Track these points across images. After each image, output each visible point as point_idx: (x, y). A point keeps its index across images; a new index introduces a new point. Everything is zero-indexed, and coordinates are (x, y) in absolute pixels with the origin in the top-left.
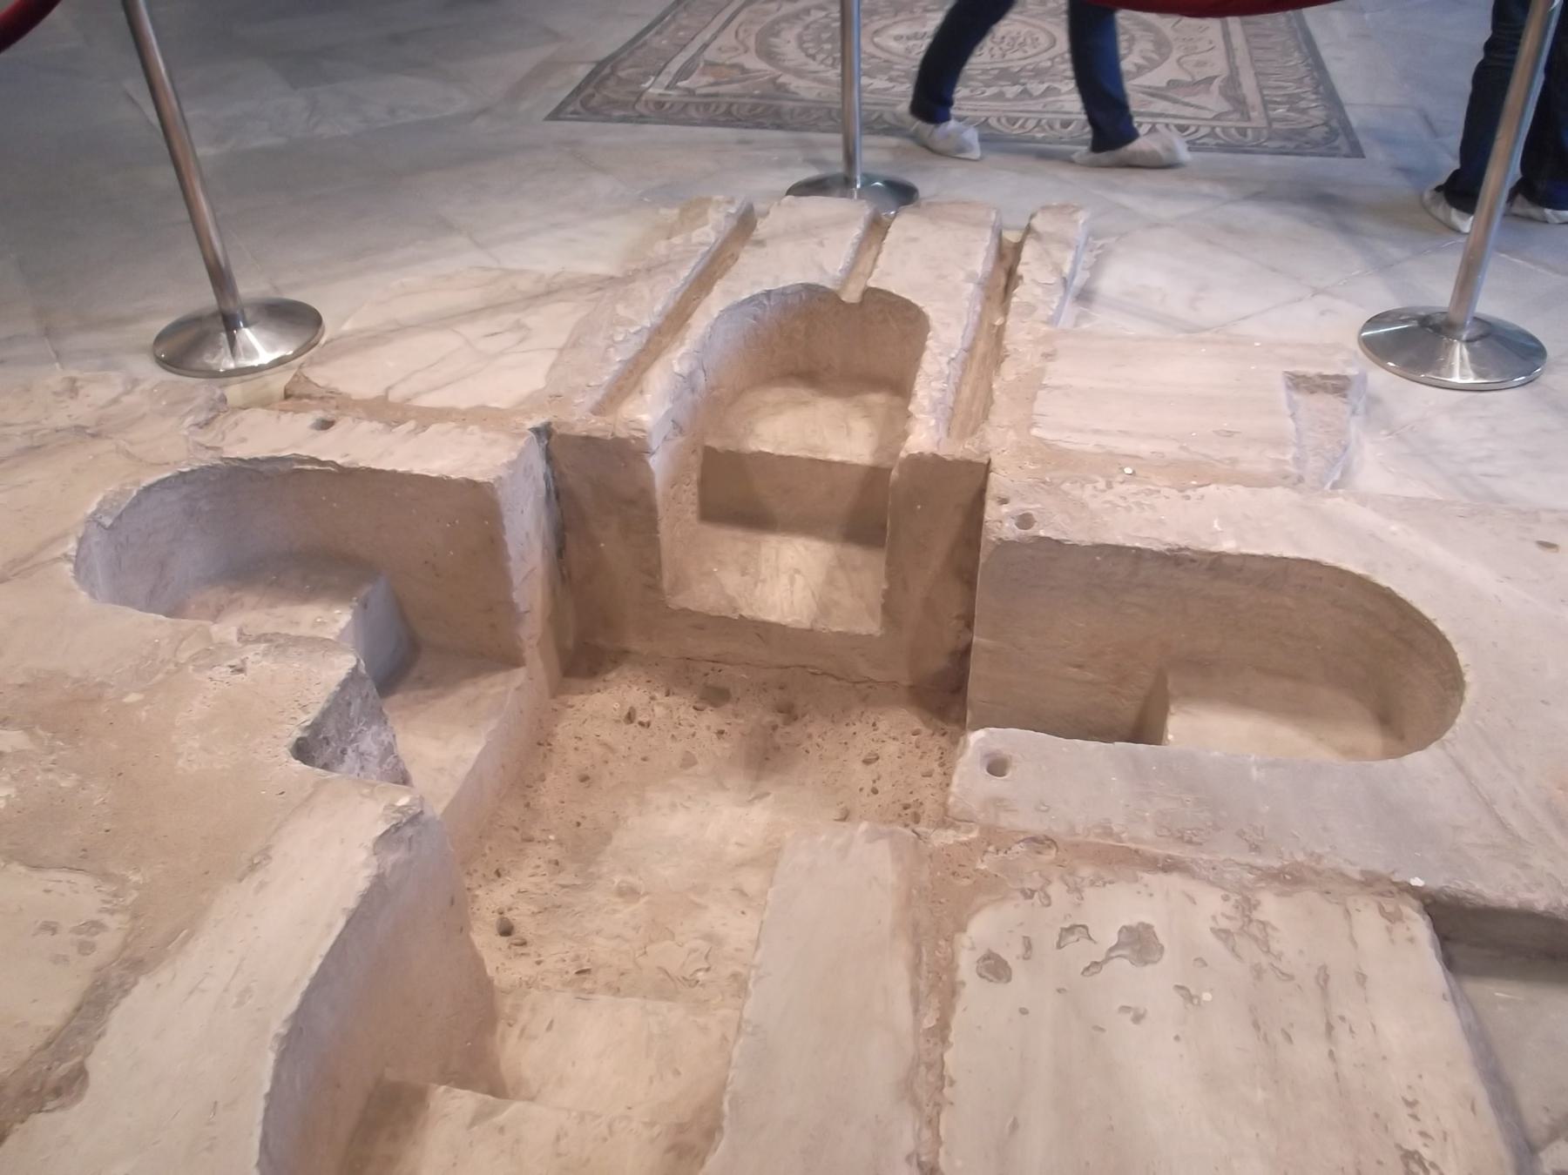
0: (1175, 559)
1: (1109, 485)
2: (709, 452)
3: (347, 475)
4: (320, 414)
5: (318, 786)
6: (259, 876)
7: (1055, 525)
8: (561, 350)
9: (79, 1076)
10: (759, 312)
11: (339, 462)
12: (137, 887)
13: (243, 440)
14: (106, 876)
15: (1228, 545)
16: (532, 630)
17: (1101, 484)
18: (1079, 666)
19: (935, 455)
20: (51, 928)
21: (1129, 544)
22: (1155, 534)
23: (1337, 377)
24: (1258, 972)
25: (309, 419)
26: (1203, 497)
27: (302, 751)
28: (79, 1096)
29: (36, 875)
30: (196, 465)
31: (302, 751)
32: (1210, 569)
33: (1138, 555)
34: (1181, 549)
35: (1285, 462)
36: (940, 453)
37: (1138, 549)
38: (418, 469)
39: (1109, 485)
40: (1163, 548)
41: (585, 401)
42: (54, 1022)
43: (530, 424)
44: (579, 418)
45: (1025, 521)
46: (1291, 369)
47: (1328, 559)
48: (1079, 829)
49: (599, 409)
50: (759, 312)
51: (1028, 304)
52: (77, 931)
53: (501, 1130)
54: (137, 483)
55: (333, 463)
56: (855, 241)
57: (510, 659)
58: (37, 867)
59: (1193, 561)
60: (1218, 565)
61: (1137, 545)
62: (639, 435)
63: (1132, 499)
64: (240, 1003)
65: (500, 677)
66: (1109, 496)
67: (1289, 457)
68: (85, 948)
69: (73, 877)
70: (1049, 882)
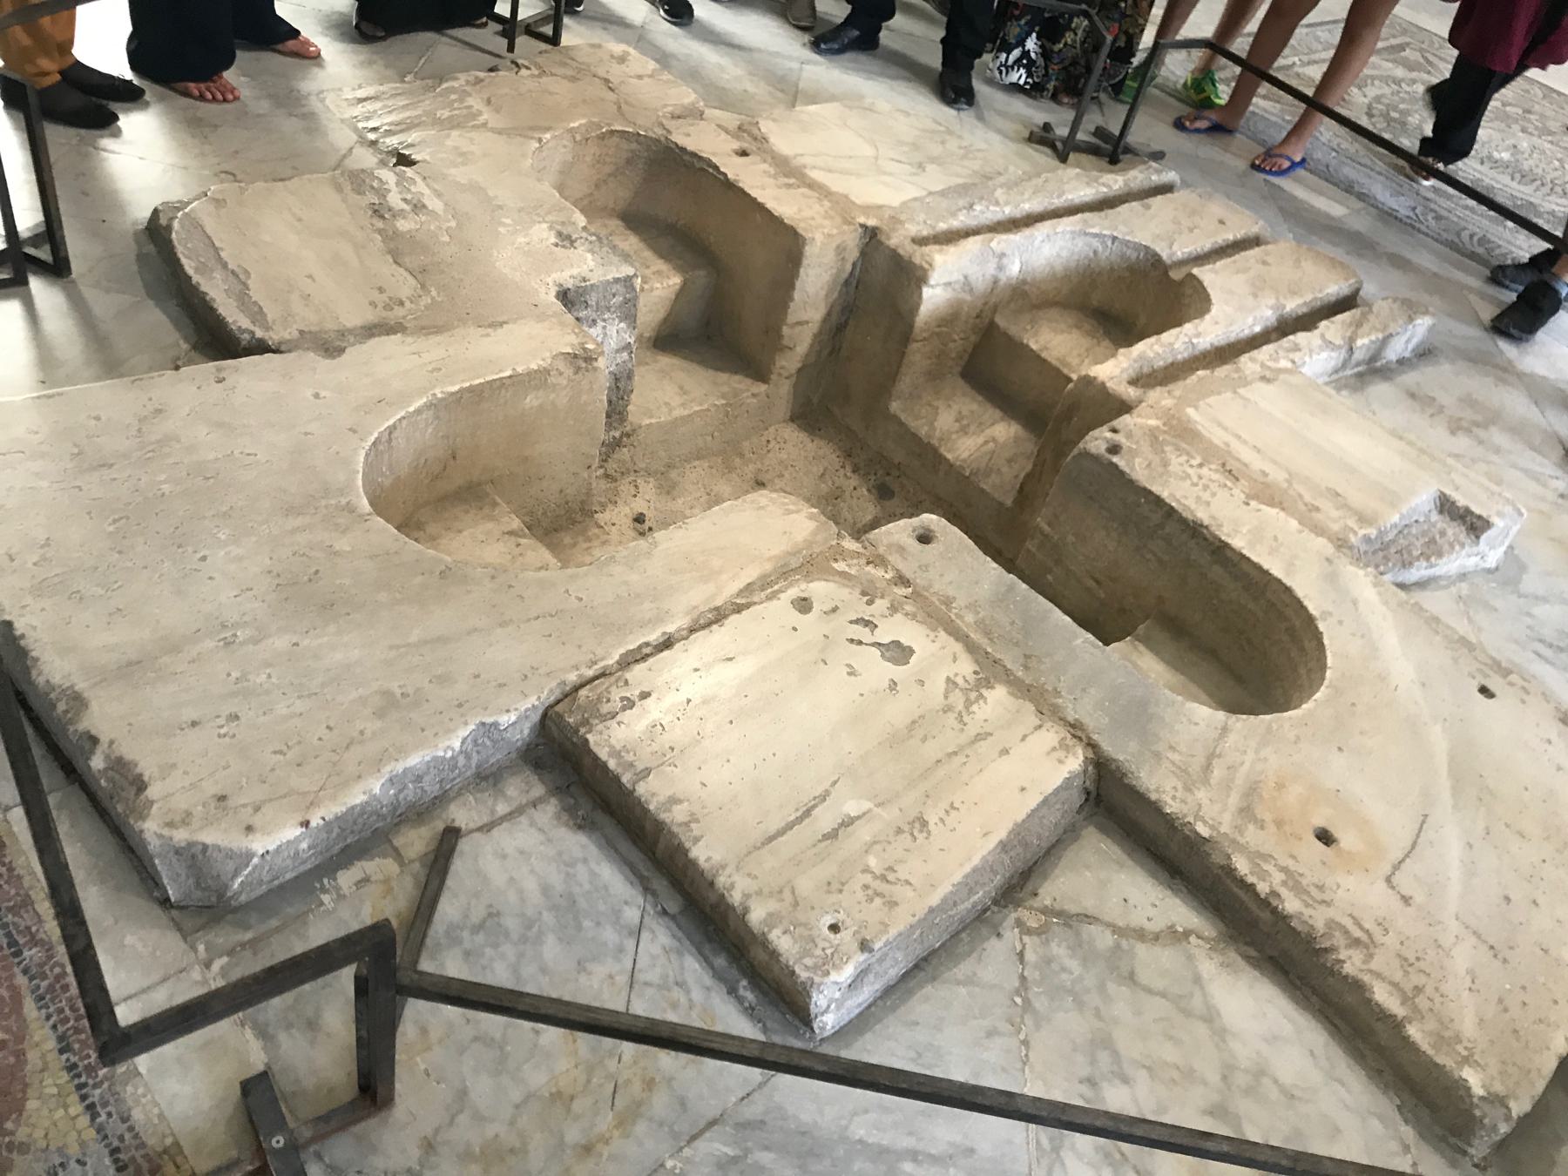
0: (1195, 531)
1: (1201, 465)
2: (992, 325)
3: (730, 187)
4: (745, 145)
5: (555, 314)
6: (489, 330)
7: (1137, 467)
8: (930, 193)
9: (341, 351)
10: (1100, 249)
11: (729, 176)
12: (433, 298)
13: (689, 135)
14: (423, 286)
15: (1237, 542)
16: (789, 363)
17: (1195, 462)
18: (1097, 582)
19: (1103, 384)
20: (381, 290)
21: (1167, 501)
22: (1193, 506)
23: (1480, 517)
24: (947, 709)
25: (736, 145)
26: (1259, 510)
27: (565, 296)
28: (334, 358)
29: (394, 266)
30: (650, 134)
31: (565, 296)
32: (1213, 552)
33: (1171, 512)
34: (1201, 525)
35: (1355, 533)
36: (1108, 385)
37: (1172, 508)
38: (771, 205)
39: (1201, 465)
40: (1190, 517)
41: (913, 229)
42: (349, 325)
43: (862, 220)
44: (897, 240)
45: (1115, 449)
46: (1448, 492)
47: (1300, 592)
48: (932, 590)
49: (921, 241)
50: (1100, 249)
51: (1296, 345)
52: (390, 299)
53: (518, 545)
54: (609, 125)
55: (725, 175)
56: (1220, 241)
57: (759, 373)
58: (396, 262)
59: (1205, 539)
60: (1221, 551)
61: (1173, 504)
62: (926, 266)
63: (1203, 481)
64: (432, 372)
65: (749, 381)
66: (1190, 471)
67: (1362, 532)
68: (388, 307)
69: (410, 278)
70: (882, 597)
